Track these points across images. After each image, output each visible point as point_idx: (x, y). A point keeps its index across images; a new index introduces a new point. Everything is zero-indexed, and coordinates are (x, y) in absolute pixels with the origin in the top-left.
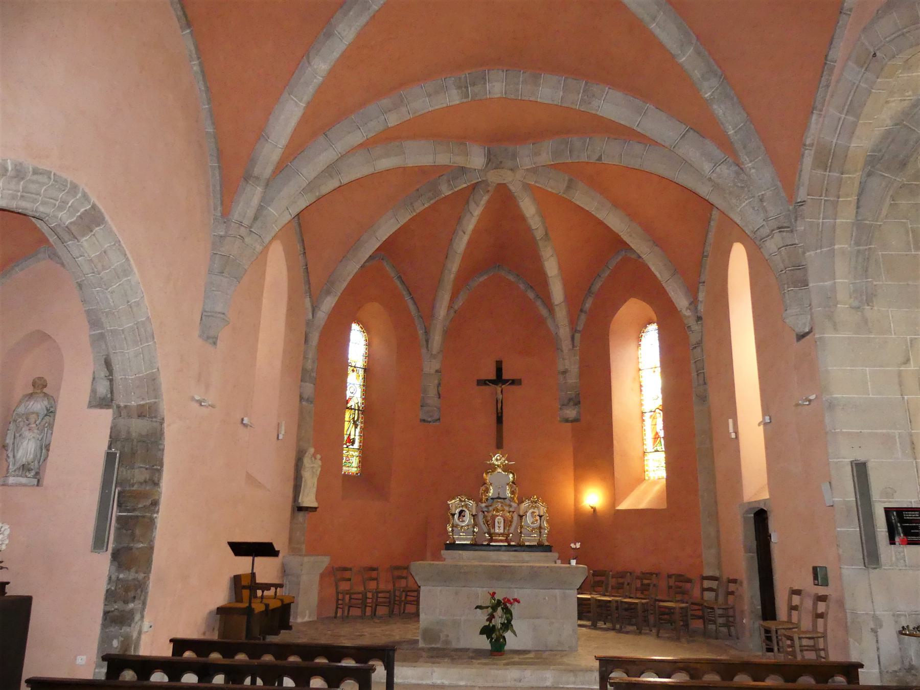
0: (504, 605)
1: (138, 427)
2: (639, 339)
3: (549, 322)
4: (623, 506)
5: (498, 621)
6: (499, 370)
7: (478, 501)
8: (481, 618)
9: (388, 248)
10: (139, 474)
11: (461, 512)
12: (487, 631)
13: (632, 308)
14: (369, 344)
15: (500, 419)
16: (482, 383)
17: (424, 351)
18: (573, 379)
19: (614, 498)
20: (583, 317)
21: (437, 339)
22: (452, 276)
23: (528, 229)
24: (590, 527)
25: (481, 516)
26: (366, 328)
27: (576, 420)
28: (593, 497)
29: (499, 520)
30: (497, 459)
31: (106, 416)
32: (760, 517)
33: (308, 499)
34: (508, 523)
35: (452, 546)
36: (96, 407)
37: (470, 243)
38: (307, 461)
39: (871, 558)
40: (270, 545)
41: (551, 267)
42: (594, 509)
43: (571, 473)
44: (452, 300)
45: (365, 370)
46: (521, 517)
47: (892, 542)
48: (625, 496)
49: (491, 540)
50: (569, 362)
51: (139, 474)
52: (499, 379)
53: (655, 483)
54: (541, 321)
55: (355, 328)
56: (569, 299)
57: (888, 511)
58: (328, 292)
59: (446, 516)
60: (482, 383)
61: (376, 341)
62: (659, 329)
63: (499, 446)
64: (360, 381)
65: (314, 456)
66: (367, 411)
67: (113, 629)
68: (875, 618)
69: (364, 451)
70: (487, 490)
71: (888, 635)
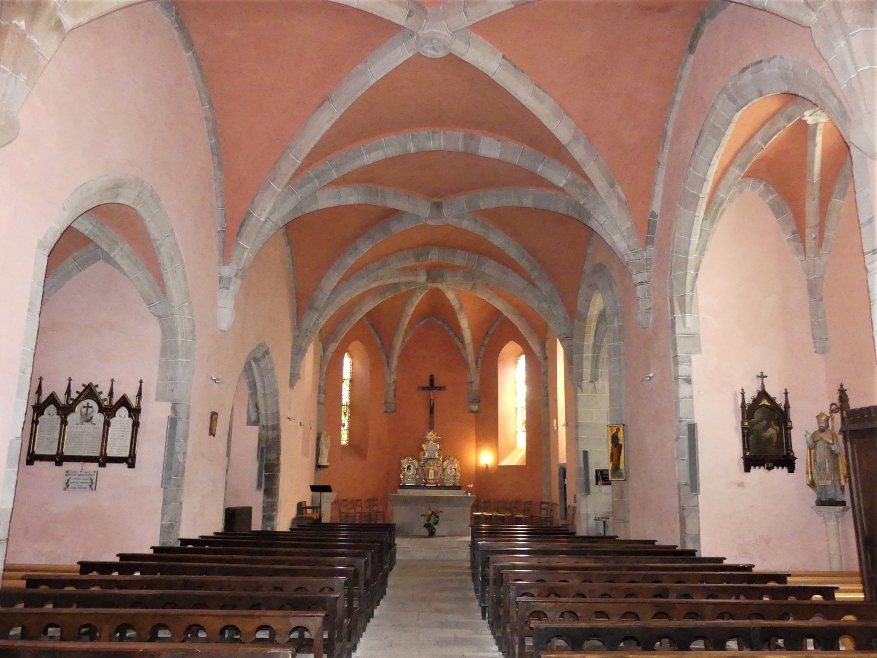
0: (435, 514)
1: (271, 434)
2: (516, 363)
3: (463, 352)
4: (504, 463)
5: (431, 522)
6: (432, 380)
7: (419, 460)
8: (424, 521)
9: (369, 315)
10: (273, 456)
11: (409, 467)
12: (427, 526)
13: (511, 347)
14: (352, 365)
15: (432, 411)
16: (424, 388)
17: (386, 368)
18: (476, 387)
19: (498, 459)
20: (483, 348)
21: (395, 362)
22: (405, 327)
23: (452, 307)
24: (484, 477)
25: (420, 469)
26: (351, 356)
27: (477, 412)
28: (485, 458)
29: (431, 472)
30: (431, 435)
31: (256, 429)
32: (563, 471)
33: (324, 461)
34: (435, 473)
35: (404, 487)
36: (251, 425)
37: (415, 311)
38: (322, 438)
39: (587, 491)
40: (329, 487)
41: (464, 323)
42: (487, 466)
43: (474, 444)
44: (404, 338)
45: (351, 381)
46: (444, 469)
47: (597, 484)
48: (504, 457)
49: (426, 483)
50: (474, 376)
51: (273, 456)
52: (432, 385)
53: (520, 451)
54: (459, 350)
55: (346, 355)
56: (475, 340)
57: (597, 471)
58: (333, 341)
59: (399, 469)
60: (424, 388)
61: (357, 364)
62: (526, 358)
63: (431, 427)
64: (348, 388)
65: (326, 436)
66: (351, 406)
67: (268, 523)
68: (587, 514)
69: (350, 430)
70: (424, 454)
71: (592, 521)
